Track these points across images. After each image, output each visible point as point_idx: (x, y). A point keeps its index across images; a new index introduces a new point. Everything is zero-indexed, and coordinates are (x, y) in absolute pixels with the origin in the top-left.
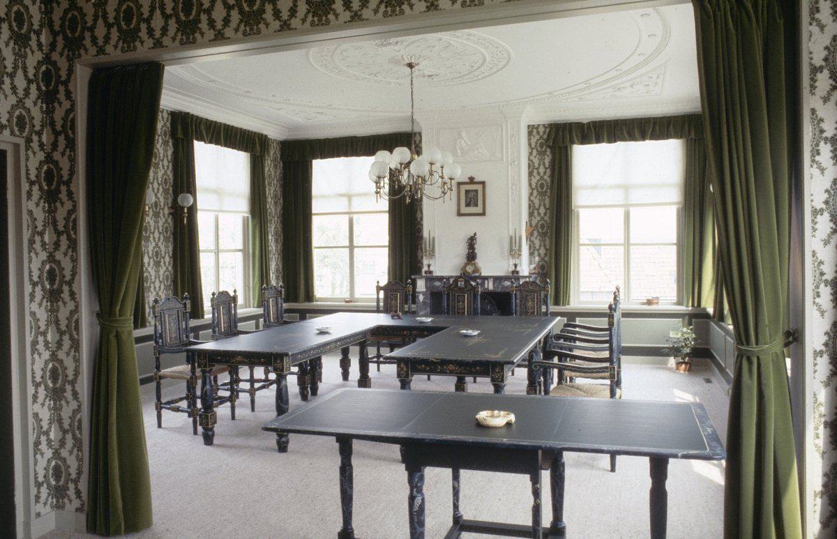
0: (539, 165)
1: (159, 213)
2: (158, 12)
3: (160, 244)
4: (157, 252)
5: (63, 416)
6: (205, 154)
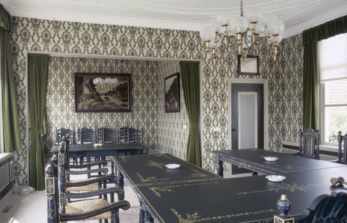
1: (291, 122)
2: (300, 58)
3: (291, 114)
4: (289, 94)
5: (39, 33)
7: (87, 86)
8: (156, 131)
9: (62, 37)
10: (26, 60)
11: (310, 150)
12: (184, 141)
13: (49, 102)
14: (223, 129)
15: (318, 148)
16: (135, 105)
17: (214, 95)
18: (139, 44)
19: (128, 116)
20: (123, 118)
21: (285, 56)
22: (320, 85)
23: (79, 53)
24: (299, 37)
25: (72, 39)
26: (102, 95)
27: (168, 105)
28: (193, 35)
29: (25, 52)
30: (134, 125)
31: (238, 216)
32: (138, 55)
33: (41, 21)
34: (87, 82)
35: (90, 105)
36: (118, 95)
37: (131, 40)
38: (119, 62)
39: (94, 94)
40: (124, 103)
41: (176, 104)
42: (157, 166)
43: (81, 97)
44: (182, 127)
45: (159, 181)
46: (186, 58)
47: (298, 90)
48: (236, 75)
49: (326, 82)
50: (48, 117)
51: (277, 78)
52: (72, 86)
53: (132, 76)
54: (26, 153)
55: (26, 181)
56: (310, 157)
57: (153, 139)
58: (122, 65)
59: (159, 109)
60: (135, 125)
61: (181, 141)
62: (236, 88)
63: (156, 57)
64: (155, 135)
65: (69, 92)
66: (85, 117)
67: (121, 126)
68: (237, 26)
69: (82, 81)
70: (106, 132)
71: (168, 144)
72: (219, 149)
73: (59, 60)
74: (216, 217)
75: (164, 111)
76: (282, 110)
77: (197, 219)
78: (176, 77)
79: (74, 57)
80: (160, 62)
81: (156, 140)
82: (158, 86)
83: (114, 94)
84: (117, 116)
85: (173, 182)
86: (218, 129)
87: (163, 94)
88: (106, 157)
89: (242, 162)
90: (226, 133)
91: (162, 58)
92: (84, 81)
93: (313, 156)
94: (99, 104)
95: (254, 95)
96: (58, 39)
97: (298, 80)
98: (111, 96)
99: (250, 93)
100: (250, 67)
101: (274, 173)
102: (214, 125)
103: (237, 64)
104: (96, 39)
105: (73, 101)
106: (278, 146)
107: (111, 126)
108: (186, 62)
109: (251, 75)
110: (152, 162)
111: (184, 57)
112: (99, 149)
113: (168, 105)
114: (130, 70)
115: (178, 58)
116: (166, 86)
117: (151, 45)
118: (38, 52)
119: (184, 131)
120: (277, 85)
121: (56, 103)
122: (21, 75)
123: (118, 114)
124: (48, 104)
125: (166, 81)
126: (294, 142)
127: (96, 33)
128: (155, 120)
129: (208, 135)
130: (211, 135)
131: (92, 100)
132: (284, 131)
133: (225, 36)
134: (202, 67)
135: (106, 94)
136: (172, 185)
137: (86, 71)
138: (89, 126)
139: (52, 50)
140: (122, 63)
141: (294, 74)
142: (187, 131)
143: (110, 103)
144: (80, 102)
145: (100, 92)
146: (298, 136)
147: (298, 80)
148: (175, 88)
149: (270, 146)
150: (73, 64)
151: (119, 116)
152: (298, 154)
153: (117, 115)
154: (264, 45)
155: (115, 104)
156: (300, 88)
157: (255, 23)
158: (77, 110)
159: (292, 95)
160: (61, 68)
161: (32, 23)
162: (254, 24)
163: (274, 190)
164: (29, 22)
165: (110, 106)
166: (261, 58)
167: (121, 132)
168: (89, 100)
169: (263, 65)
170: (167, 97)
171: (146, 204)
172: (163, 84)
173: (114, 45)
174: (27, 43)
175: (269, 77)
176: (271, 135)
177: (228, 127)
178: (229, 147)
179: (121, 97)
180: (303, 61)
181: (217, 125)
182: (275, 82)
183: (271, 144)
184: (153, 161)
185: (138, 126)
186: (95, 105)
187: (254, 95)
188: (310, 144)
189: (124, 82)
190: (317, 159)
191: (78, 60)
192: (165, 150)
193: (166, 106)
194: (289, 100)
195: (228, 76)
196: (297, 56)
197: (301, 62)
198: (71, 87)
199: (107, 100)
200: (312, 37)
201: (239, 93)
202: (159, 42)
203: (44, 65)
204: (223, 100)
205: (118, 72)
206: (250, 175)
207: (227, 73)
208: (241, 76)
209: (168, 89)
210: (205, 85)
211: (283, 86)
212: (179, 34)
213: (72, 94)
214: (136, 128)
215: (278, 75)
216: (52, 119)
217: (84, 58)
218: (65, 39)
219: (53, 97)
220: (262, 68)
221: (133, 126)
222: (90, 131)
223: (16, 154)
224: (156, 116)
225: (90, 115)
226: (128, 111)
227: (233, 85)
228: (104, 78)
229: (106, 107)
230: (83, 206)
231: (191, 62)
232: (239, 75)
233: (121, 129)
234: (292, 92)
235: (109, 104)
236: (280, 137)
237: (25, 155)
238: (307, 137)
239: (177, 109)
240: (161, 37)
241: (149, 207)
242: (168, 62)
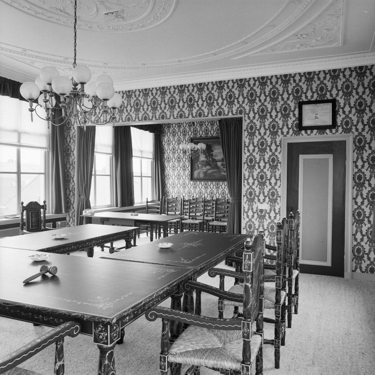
6: (204, 296)
13: (167, 170)
14: (273, 208)
19: (200, 186)
20: (195, 188)
21: (99, 114)
26: (219, 161)
29: (76, 126)
35: (205, 173)
39: (210, 161)
46: (224, 115)
48: (296, 131)
50: (167, 185)
54: (74, 217)
62: (294, 151)
63: (207, 116)
66: (200, 185)
86: (265, 206)
91: (194, 118)
94: (215, 171)
95: (328, 159)
100: (319, 117)
102: (259, 200)
103: (297, 116)
105: (189, 168)
108: (226, 120)
109: (321, 129)
111: (220, 114)
115: (213, 116)
117: (222, 101)
121: (174, 170)
122: (72, 147)
123: (201, 184)
124: (167, 172)
130: (254, 213)
131: (208, 167)
134: (245, 125)
137: (202, 136)
144: (196, 170)
145: (216, 158)
151: (214, 186)
153: (223, 185)
158: (192, 178)
166: (342, 102)
168: (205, 167)
181: (264, 200)
186: (211, 172)
187: (328, 159)
195: (282, 133)
204: (274, 167)
208: (303, 132)
216: (169, 187)
219: (171, 164)
221: (206, 197)
223: (68, 216)
225: (217, 184)
227: (290, 145)
231: (232, 119)
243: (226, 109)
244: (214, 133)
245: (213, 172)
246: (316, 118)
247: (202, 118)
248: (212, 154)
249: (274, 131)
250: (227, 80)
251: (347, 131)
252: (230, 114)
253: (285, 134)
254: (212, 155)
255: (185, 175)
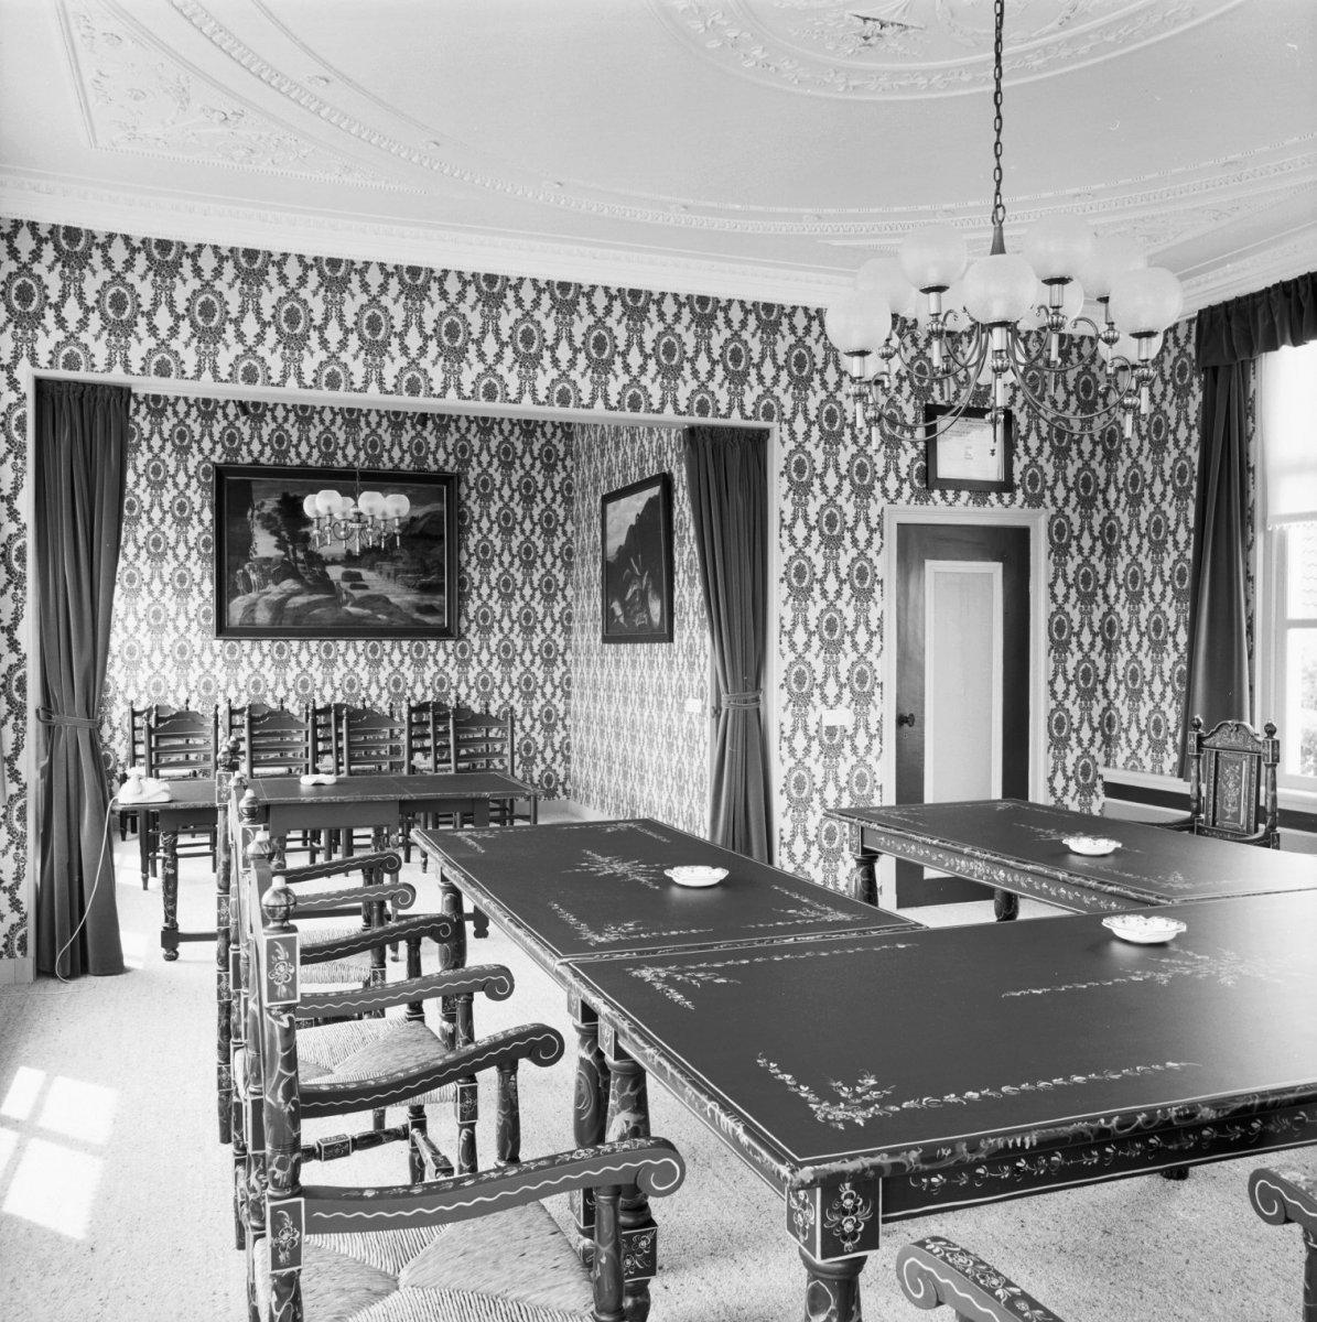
0: (407, 326)
7: (268, 523)
8: (563, 720)
9: (187, 310)
10: (29, 408)
11: (1235, 809)
12: (691, 764)
15: (1274, 799)
16: (472, 607)
17: (826, 573)
18: (440, 344)
22: (1268, 535)
23: (83, 367)
24: (1181, 333)
25: (50, 305)
26: (334, 562)
27: (619, 612)
28: (805, 322)
30: (468, 696)
31: (1046, 1091)
32: (513, 396)
33: (94, 237)
34: (270, 505)
35: (278, 608)
36: (400, 565)
37: (484, 333)
38: (408, 422)
39: (297, 560)
40: (427, 600)
41: (655, 607)
42: (625, 876)
43: (240, 571)
44: (681, 706)
45: (661, 941)
46: (715, 416)
47: (1175, 555)
48: (919, 491)
49: (1294, 524)
51: (1087, 503)
52: (201, 521)
53: (463, 485)
54: (22, 816)
55: (23, 939)
56: (1239, 837)
57: (549, 754)
58: (419, 434)
59: (576, 625)
60: (474, 693)
61: (674, 763)
63: (587, 407)
64: (557, 739)
65: (139, 548)
67: (414, 695)
68: (1001, 292)
69: (248, 503)
70: (352, 724)
71: (616, 778)
72: (846, 803)
73: (148, 406)
74: (960, 1094)
75: (599, 636)
76: (1104, 639)
77: (883, 1102)
78: (655, 491)
79: (212, 397)
80: (583, 427)
81: (559, 757)
82: (569, 527)
83: (383, 559)
84: (396, 653)
85: (722, 946)
86: (842, 717)
87: (595, 562)
88: (356, 832)
89: (970, 857)
90: (873, 731)
91: (613, 414)
92: (257, 504)
93: (1249, 831)
95: (990, 575)
96: (340, 335)
97: (1172, 513)
98: (371, 568)
99: (974, 564)
101: (1114, 905)
102: (824, 698)
104: (333, 324)
105: (209, 587)
106: (1086, 790)
107: (369, 696)
108: (713, 431)
109: (980, 490)
110: (599, 858)
111: (703, 409)
112: (325, 799)
113: (619, 612)
114: (268, 451)
116: (610, 529)
118: (82, 375)
119: (690, 721)
120: (1086, 533)
125: (610, 506)
126: (1153, 771)
127: (72, 273)
128: (557, 675)
129: (800, 742)
130: (811, 739)
131: (289, 584)
132: (1110, 725)
133: (932, 333)
135: (349, 559)
136: (722, 956)
137: (263, 460)
138: (275, 698)
139: (50, 362)
140: (419, 427)
141: (1158, 488)
142: (702, 724)
143: (370, 597)
144: (236, 593)
145: (325, 551)
146: (1170, 747)
147: (1172, 513)
148: (654, 533)
149: (1053, 790)
150: (207, 429)
151: (404, 655)
152: (1186, 826)
154: (1087, 369)
155: (387, 601)
156: (1182, 546)
157: (1062, 281)
158: (223, 629)
159: (1148, 575)
160: (156, 442)
161: (57, 247)
162: (1056, 286)
163: (1153, 978)
164: (41, 241)
165: (367, 612)
166: (1022, 419)
167: (411, 725)
169: (1027, 450)
170: (614, 577)
171: (646, 1042)
172: (597, 520)
173: (413, 353)
174: (34, 334)
175: (1054, 500)
176: (1058, 743)
177: (885, 709)
178: (888, 797)
179: (414, 572)
180: (1196, 436)
181: (839, 697)
182: (1076, 520)
183: (1059, 782)
184: (604, 856)
185: (486, 697)
186: (303, 605)
187: (990, 575)
188: (1238, 784)
189: (428, 509)
190: (1267, 845)
191: (231, 410)
192: (602, 802)
193: (608, 614)
194: (1135, 598)
195: (885, 491)
196: (1172, 412)
197: (1188, 440)
198: (200, 529)
199: (354, 587)
200: (1229, 340)
201: (929, 564)
202: (452, 331)
203: (107, 431)
205: (403, 466)
206: (982, 913)
207: (882, 480)
208: (936, 494)
209: (617, 540)
210: (790, 527)
211: (1109, 539)
212: (394, 284)
213: (202, 557)
214: (477, 709)
215: (1087, 493)
217: (256, 405)
218: (199, 319)
220: (1026, 460)
221: (463, 697)
222: (280, 718)
224: (563, 655)
226: (442, 634)
227: (904, 530)
228: (353, 493)
229: (349, 613)
230: (325, 1047)
231: (733, 430)
232: (929, 489)
233: (411, 710)
234: (1148, 566)
235: (359, 603)
236: (1093, 751)
237: (17, 825)
238: (1223, 754)
239: (661, 628)
240: (461, 311)
241: (662, 1055)
242: (617, 429)
243: (723, 397)
244: (446, 462)
245: (316, 604)
246: (968, 457)
247: (641, 415)
248: (307, 534)
249: (863, 483)
250: (514, 275)
251: (1034, 501)
252: (736, 413)
253: (892, 495)
254: (307, 538)
255: (806, 623)
